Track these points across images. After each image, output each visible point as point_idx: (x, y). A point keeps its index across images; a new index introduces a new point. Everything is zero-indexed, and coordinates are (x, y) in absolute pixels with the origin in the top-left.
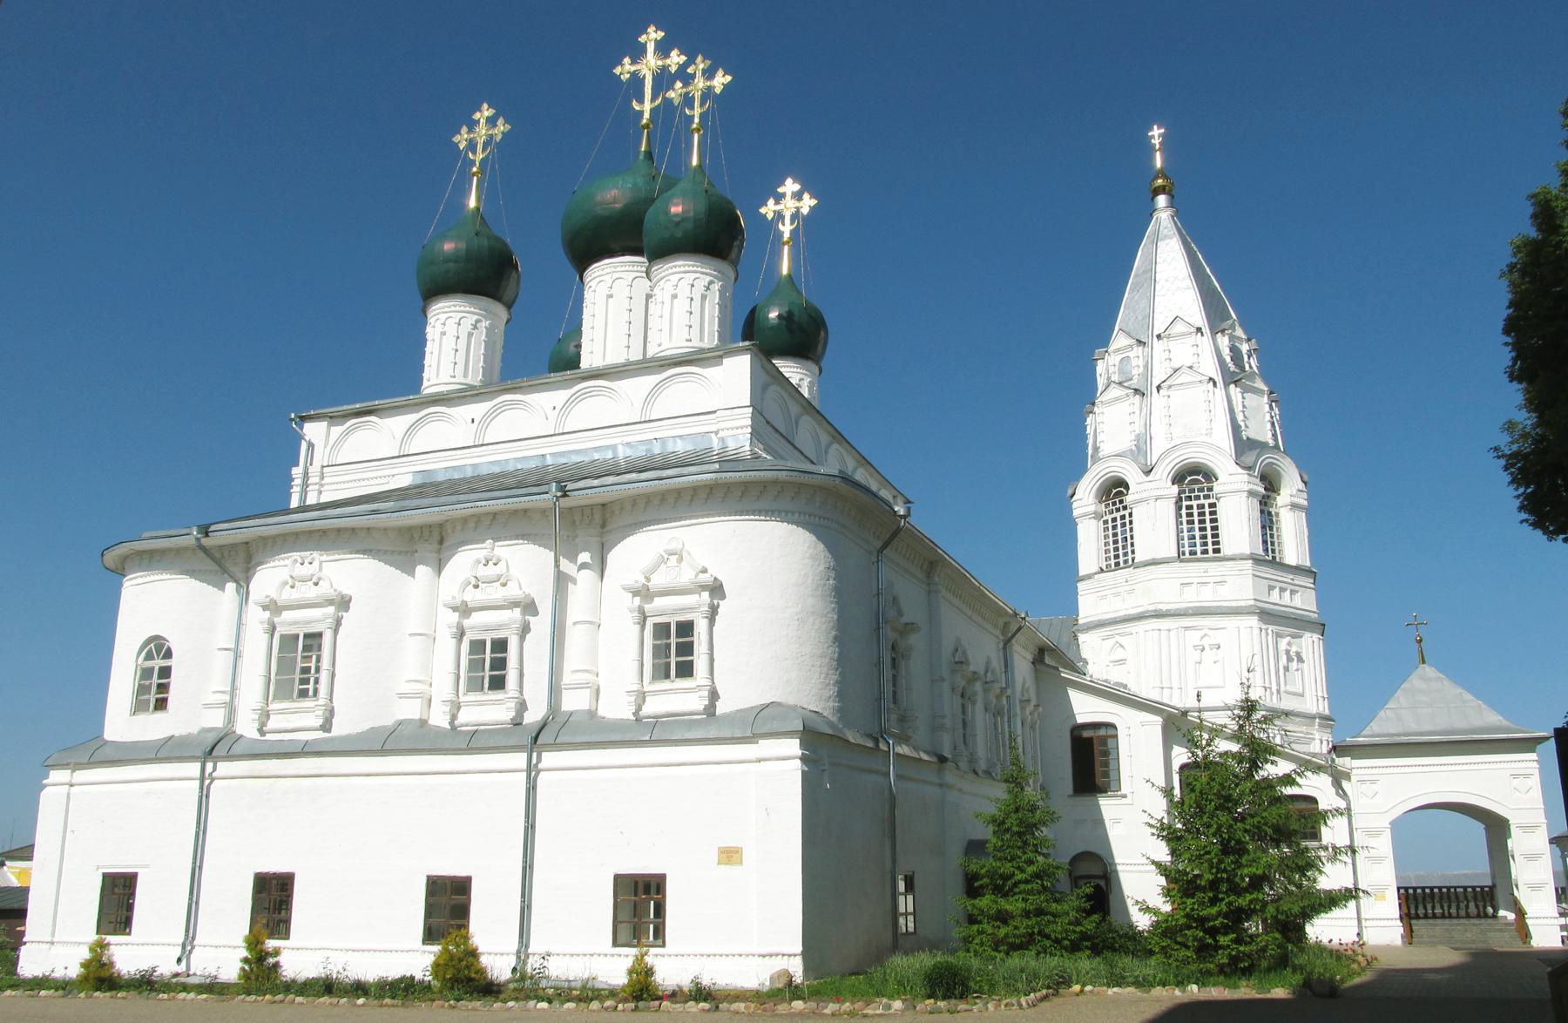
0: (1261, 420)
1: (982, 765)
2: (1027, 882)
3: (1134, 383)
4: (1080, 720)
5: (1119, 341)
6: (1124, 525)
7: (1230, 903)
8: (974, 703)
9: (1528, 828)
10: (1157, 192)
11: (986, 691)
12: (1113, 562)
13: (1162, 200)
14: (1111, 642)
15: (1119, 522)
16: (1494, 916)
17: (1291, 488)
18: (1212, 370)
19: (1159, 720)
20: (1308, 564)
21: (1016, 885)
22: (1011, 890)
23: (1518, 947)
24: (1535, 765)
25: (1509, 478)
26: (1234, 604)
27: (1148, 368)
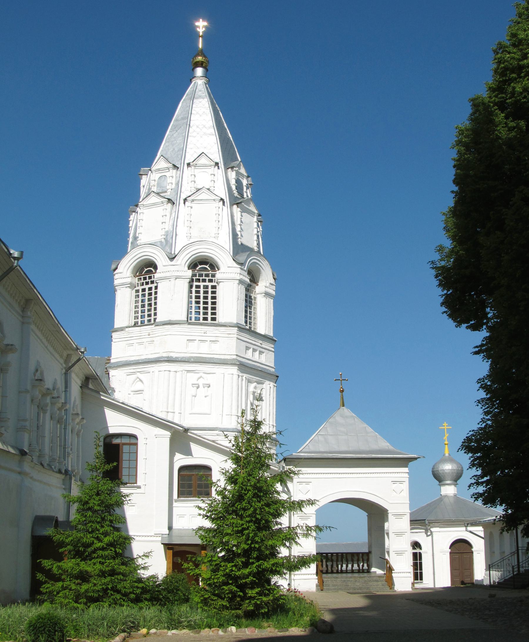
0: (251, 234)
1: (46, 460)
2: (103, 549)
3: (168, 195)
4: (112, 431)
5: (159, 163)
6: (150, 294)
7: (259, 566)
8: (45, 412)
9: (399, 516)
10: (197, 64)
11: (53, 404)
12: (146, 319)
13: (199, 71)
14: (134, 377)
15: (147, 292)
16: (368, 571)
17: (266, 282)
18: (223, 193)
19: (168, 434)
20: (271, 334)
21: (94, 551)
22: (90, 555)
23: (387, 592)
24: (407, 475)
25: (437, 283)
26: (222, 357)
27: (179, 185)
